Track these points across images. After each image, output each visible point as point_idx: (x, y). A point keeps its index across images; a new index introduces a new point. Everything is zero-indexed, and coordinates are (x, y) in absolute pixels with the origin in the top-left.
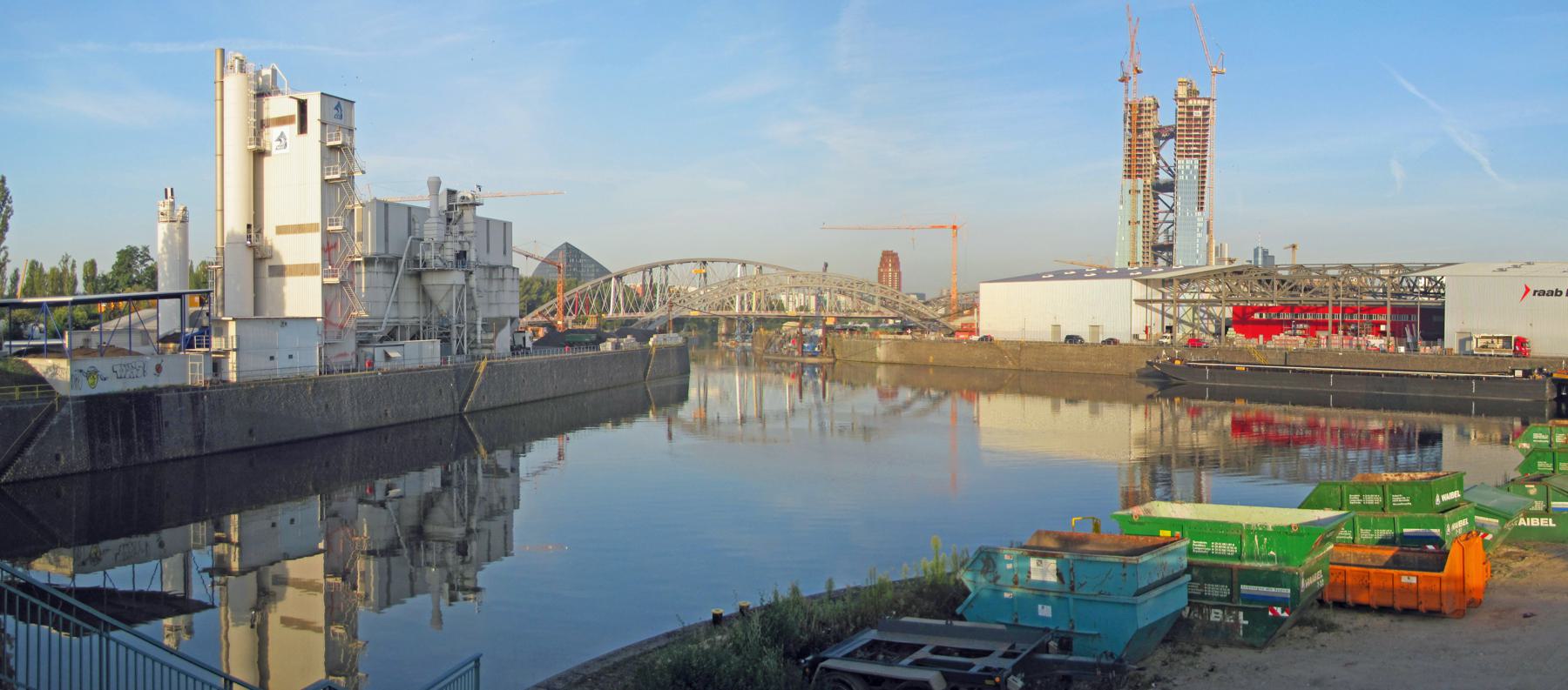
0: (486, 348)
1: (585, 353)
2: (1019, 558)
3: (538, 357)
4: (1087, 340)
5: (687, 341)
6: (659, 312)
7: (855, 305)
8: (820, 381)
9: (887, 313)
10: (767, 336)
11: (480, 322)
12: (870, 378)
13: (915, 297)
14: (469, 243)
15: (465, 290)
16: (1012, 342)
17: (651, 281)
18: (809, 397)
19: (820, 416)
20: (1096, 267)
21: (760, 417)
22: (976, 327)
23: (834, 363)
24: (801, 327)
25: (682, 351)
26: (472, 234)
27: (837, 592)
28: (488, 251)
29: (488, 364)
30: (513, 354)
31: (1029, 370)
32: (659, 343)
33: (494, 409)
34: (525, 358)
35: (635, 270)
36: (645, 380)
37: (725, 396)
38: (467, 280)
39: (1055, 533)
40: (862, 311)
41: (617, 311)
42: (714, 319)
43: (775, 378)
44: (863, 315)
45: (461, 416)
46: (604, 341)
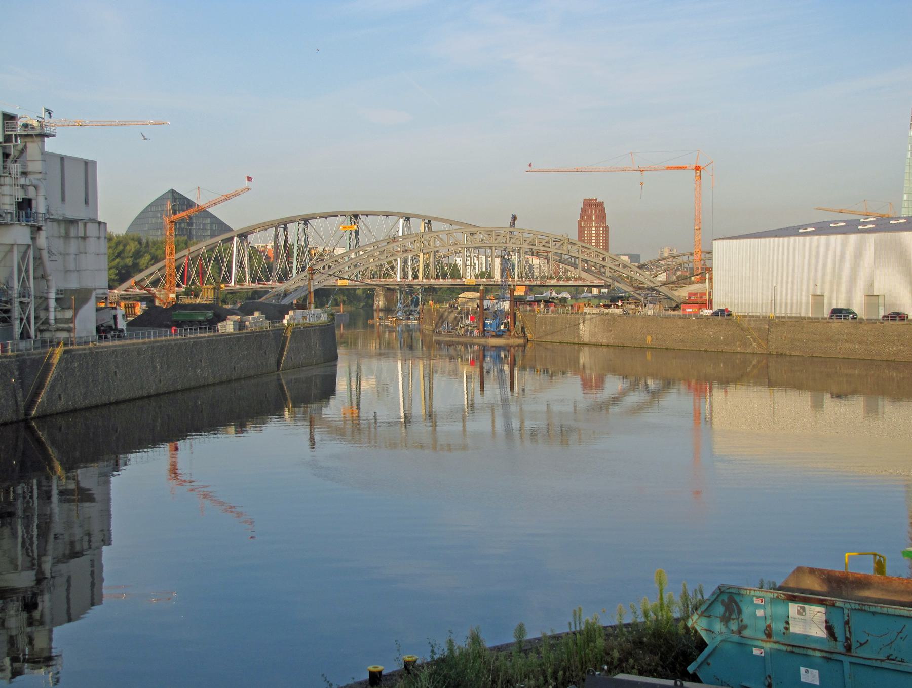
0: (62, 330)
1: (199, 335)
2: (772, 601)
3: (135, 341)
4: (862, 314)
5: (333, 319)
6: (296, 280)
7: (553, 269)
8: (506, 368)
9: (590, 279)
10: (438, 311)
11: (52, 295)
12: (573, 366)
13: (626, 259)
14: (36, 187)
15: (31, 253)
16: (758, 317)
17: (286, 241)
18: (493, 391)
19: (507, 416)
20: (875, 217)
21: (430, 416)
22: (707, 297)
23: (525, 346)
24: (482, 299)
25: (327, 333)
26: (39, 176)
27: (530, 641)
28: (63, 199)
29: (65, 352)
30: (100, 338)
31: (780, 355)
32: (296, 322)
33: (75, 411)
34: (117, 343)
35: (264, 227)
36: (278, 370)
37: (383, 390)
38: (33, 239)
39: (821, 572)
40: (560, 278)
41: (240, 280)
42: (369, 289)
43: (448, 365)
44: (562, 283)
45: (26, 422)
46: (224, 319)
